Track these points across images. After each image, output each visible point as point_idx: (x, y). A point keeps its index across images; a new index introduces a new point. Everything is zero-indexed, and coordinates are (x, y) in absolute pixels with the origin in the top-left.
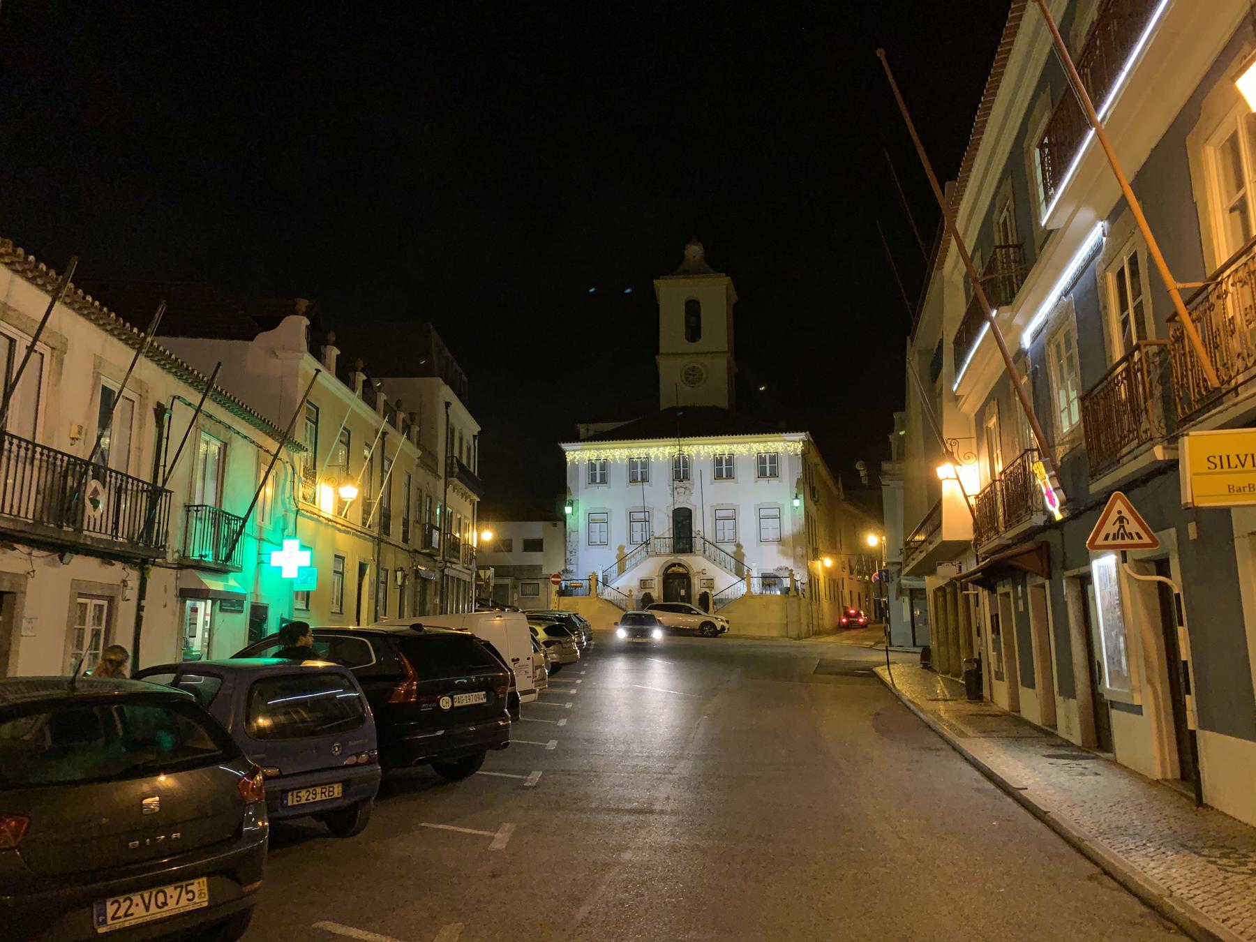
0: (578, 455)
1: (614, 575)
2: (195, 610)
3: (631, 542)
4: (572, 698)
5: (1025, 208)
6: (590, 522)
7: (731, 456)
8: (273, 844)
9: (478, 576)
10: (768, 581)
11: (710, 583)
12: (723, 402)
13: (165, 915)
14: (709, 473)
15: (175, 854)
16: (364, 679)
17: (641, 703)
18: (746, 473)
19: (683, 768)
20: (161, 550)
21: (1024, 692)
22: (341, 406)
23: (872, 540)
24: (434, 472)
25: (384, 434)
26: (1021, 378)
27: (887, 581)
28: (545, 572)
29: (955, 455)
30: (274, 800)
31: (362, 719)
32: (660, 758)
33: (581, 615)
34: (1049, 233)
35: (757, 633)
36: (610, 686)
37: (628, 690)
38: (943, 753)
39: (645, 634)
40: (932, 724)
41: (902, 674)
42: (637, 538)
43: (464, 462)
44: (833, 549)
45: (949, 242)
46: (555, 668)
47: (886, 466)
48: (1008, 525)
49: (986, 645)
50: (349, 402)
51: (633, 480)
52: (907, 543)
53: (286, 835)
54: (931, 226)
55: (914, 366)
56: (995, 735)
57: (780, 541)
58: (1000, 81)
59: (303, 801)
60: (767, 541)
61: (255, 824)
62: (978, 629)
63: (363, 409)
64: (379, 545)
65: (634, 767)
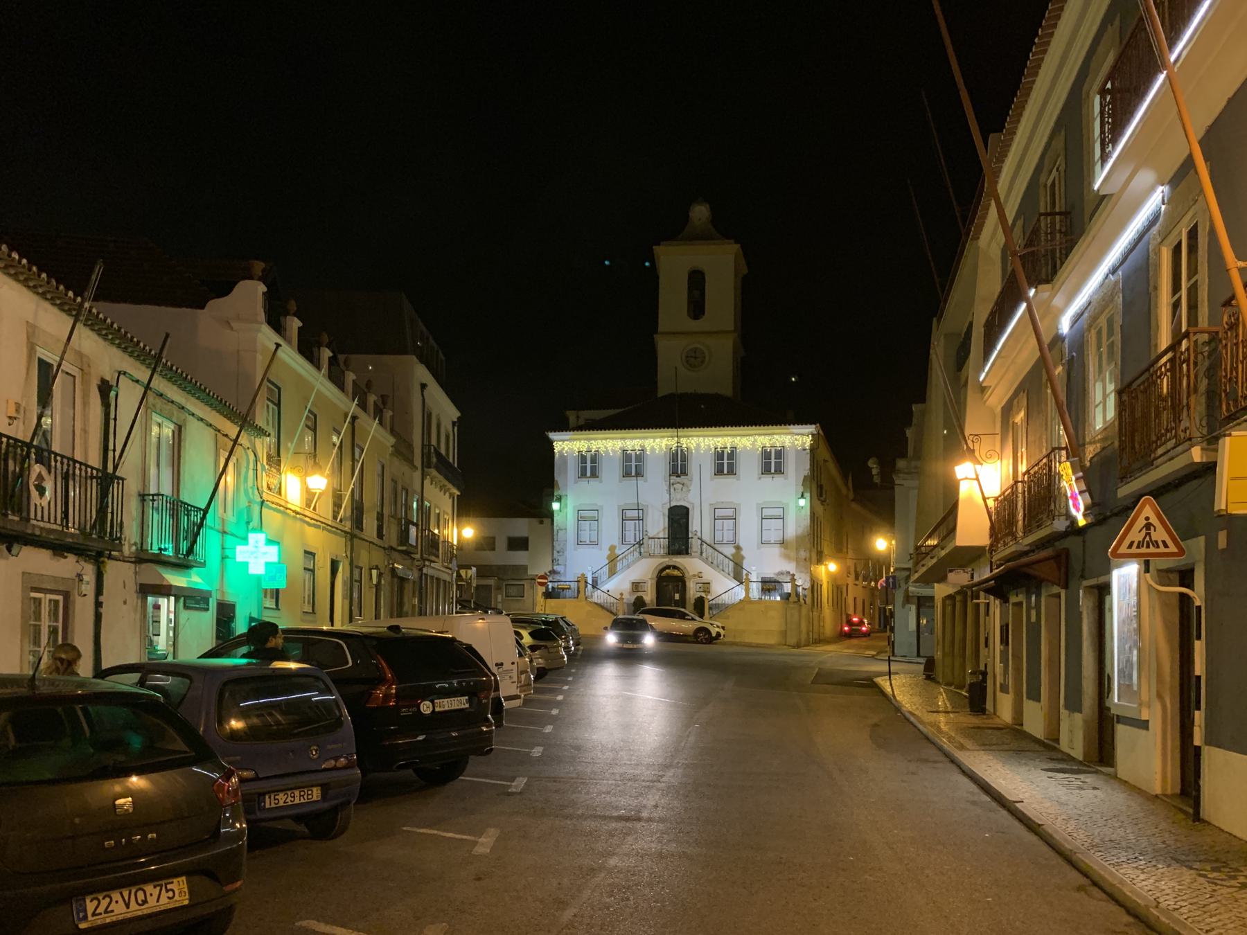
0: (567, 445)
1: (605, 577)
2: (157, 607)
3: (623, 541)
4: (558, 704)
6: (580, 519)
7: (734, 449)
9: (459, 576)
10: (767, 586)
11: (706, 587)
12: (725, 388)
13: (145, 912)
14: (709, 467)
16: (341, 681)
17: (630, 711)
18: (749, 468)
20: (117, 542)
22: (303, 386)
23: (881, 544)
24: (410, 461)
25: (354, 418)
26: (1055, 367)
27: (894, 587)
29: (977, 454)
30: (251, 803)
31: (339, 723)
32: (648, 766)
34: (1102, 199)
37: (618, 697)
39: (636, 639)
40: (930, 735)
42: (630, 537)
43: (443, 452)
44: (839, 551)
46: (541, 674)
47: (901, 464)
51: (627, 474)
52: (917, 548)
53: (266, 836)
54: (970, 186)
57: (783, 543)
59: (281, 803)
61: (233, 826)
62: (987, 640)
64: (351, 540)
65: (621, 775)
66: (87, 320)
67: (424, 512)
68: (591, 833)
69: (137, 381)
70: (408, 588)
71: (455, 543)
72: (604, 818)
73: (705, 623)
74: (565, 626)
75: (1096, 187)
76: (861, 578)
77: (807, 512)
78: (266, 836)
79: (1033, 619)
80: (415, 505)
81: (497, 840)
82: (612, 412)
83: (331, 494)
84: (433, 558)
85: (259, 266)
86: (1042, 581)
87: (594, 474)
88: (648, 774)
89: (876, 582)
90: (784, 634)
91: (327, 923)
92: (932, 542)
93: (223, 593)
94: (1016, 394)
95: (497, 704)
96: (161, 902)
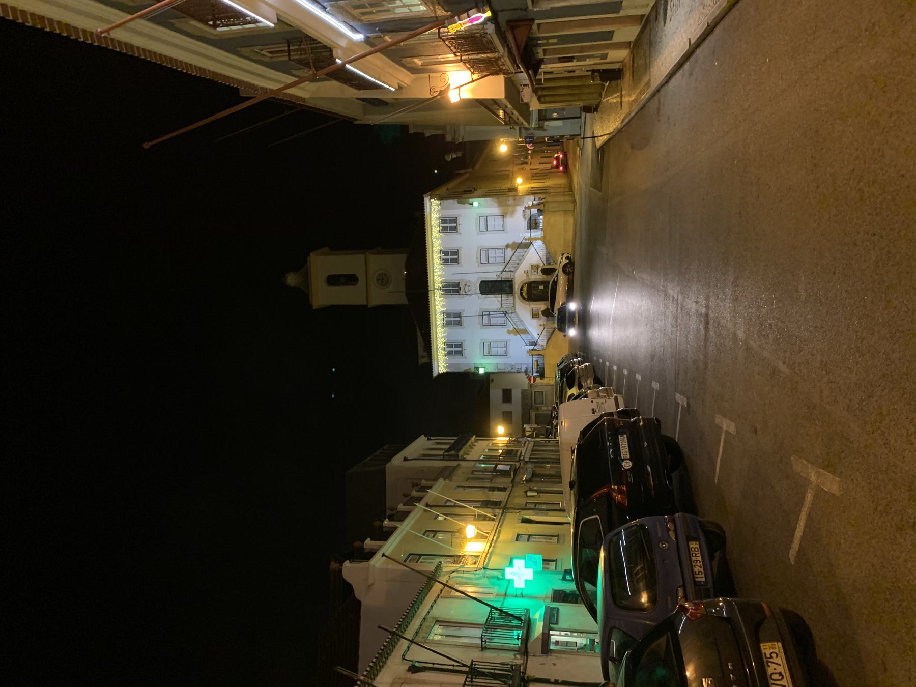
0: (441, 364)
1: (529, 337)
2: (557, 643)
5: (260, 38)
6: (490, 354)
7: (441, 252)
8: (733, 594)
9: (529, 436)
10: (533, 225)
11: (534, 267)
12: (402, 258)
13: (788, 674)
14: (454, 268)
15: (743, 665)
16: (611, 525)
17: (623, 318)
18: (454, 242)
20: (514, 668)
21: (616, 39)
22: (407, 538)
23: (503, 148)
24: (455, 468)
25: (427, 505)
26: (385, 41)
27: (532, 137)
28: (526, 387)
30: (701, 592)
31: (642, 527)
33: (559, 361)
34: (280, 21)
35: (570, 233)
36: (611, 340)
37: (614, 328)
39: (572, 315)
40: (639, 107)
42: (502, 320)
43: (447, 447)
44: (509, 177)
45: (285, 94)
46: (598, 381)
47: (449, 138)
48: (494, 50)
51: (459, 323)
52: (506, 124)
53: (724, 582)
54: (275, 107)
56: (648, 61)
57: (503, 216)
58: (166, 57)
59: (702, 570)
60: (504, 225)
61: (722, 607)
62: (569, 72)
64: (508, 509)
65: (673, 327)
67: (488, 459)
69: (408, 648)
70: (539, 471)
72: (706, 339)
73: (559, 268)
74: (563, 365)
75: (272, 25)
78: (724, 582)
79: (555, 41)
81: (725, 416)
82: (419, 334)
84: (519, 453)
85: (334, 565)
86: (529, 37)
88: (672, 308)
89: (528, 150)
90: (566, 212)
91: (792, 542)
92: (501, 113)
93: (546, 598)
94: (403, 66)
95: (621, 413)
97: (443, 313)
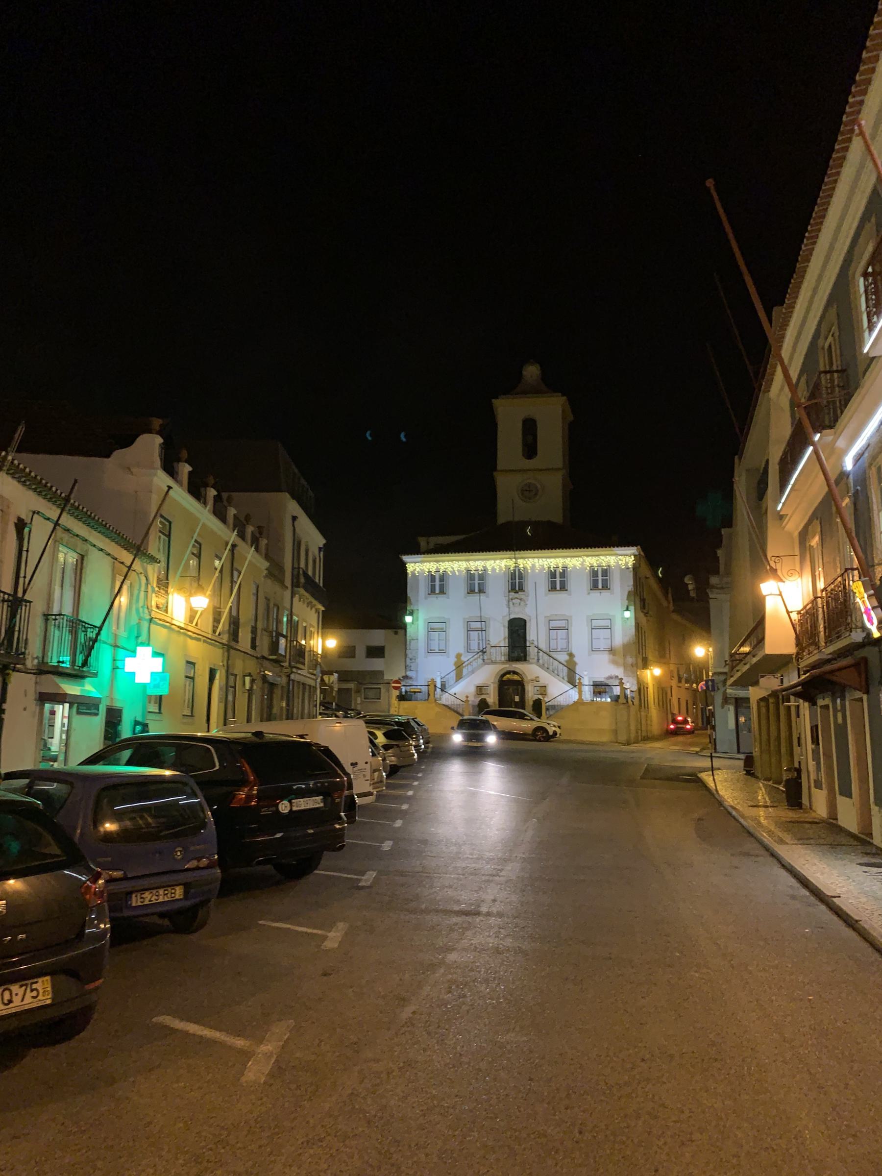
0: (418, 566)
1: (452, 682)
2: (53, 713)
3: (468, 650)
4: (408, 799)
5: (850, 335)
6: (430, 630)
7: (565, 568)
9: (322, 680)
11: (543, 690)
12: (557, 517)
13: (10, 1011)
14: (543, 585)
16: (205, 784)
17: (475, 804)
18: (579, 586)
19: (512, 870)
20: (21, 656)
22: (192, 520)
23: (700, 651)
24: (282, 582)
25: (234, 546)
26: (843, 500)
27: (713, 690)
29: (779, 573)
30: (117, 901)
31: (204, 825)
32: (489, 860)
36: (446, 788)
38: (760, 859)
39: (480, 738)
40: (752, 830)
41: (726, 780)
42: (474, 646)
43: (310, 573)
44: (662, 658)
46: (393, 771)
47: (714, 580)
48: (829, 640)
49: (806, 754)
50: (198, 515)
51: (471, 591)
52: (731, 655)
53: (130, 931)
54: (759, 352)
55: (742, 485)
56: (812, 841)
57: (611, 651)
59: (147, 902)
60: (598, 650)
61: (97, 927)
62: (799, 739)
63: (214, 523)
64: (228, 651)
66: (8, 470)
67: (293, 626)
68: (433, 928)
69: (48, 519)
70: (278, 692)
71: (320, 652)
75: (865, 351)
76: (683, 681)
77: (632, 623)
78: (130, 931)
80: (285, 619)
83: (211, 611)
87: (442, 592)
88: (489, 868)
90: (615, 732)
91: (182, 1020)
92: (746, 649)
96: (25, 1002)
97: (485, 570)
